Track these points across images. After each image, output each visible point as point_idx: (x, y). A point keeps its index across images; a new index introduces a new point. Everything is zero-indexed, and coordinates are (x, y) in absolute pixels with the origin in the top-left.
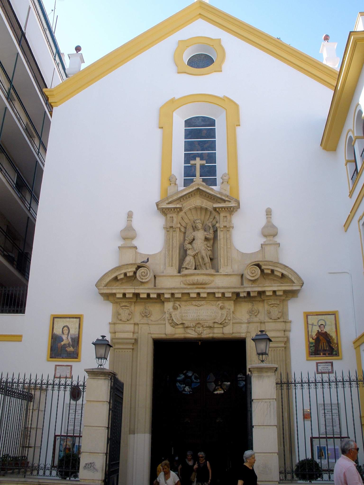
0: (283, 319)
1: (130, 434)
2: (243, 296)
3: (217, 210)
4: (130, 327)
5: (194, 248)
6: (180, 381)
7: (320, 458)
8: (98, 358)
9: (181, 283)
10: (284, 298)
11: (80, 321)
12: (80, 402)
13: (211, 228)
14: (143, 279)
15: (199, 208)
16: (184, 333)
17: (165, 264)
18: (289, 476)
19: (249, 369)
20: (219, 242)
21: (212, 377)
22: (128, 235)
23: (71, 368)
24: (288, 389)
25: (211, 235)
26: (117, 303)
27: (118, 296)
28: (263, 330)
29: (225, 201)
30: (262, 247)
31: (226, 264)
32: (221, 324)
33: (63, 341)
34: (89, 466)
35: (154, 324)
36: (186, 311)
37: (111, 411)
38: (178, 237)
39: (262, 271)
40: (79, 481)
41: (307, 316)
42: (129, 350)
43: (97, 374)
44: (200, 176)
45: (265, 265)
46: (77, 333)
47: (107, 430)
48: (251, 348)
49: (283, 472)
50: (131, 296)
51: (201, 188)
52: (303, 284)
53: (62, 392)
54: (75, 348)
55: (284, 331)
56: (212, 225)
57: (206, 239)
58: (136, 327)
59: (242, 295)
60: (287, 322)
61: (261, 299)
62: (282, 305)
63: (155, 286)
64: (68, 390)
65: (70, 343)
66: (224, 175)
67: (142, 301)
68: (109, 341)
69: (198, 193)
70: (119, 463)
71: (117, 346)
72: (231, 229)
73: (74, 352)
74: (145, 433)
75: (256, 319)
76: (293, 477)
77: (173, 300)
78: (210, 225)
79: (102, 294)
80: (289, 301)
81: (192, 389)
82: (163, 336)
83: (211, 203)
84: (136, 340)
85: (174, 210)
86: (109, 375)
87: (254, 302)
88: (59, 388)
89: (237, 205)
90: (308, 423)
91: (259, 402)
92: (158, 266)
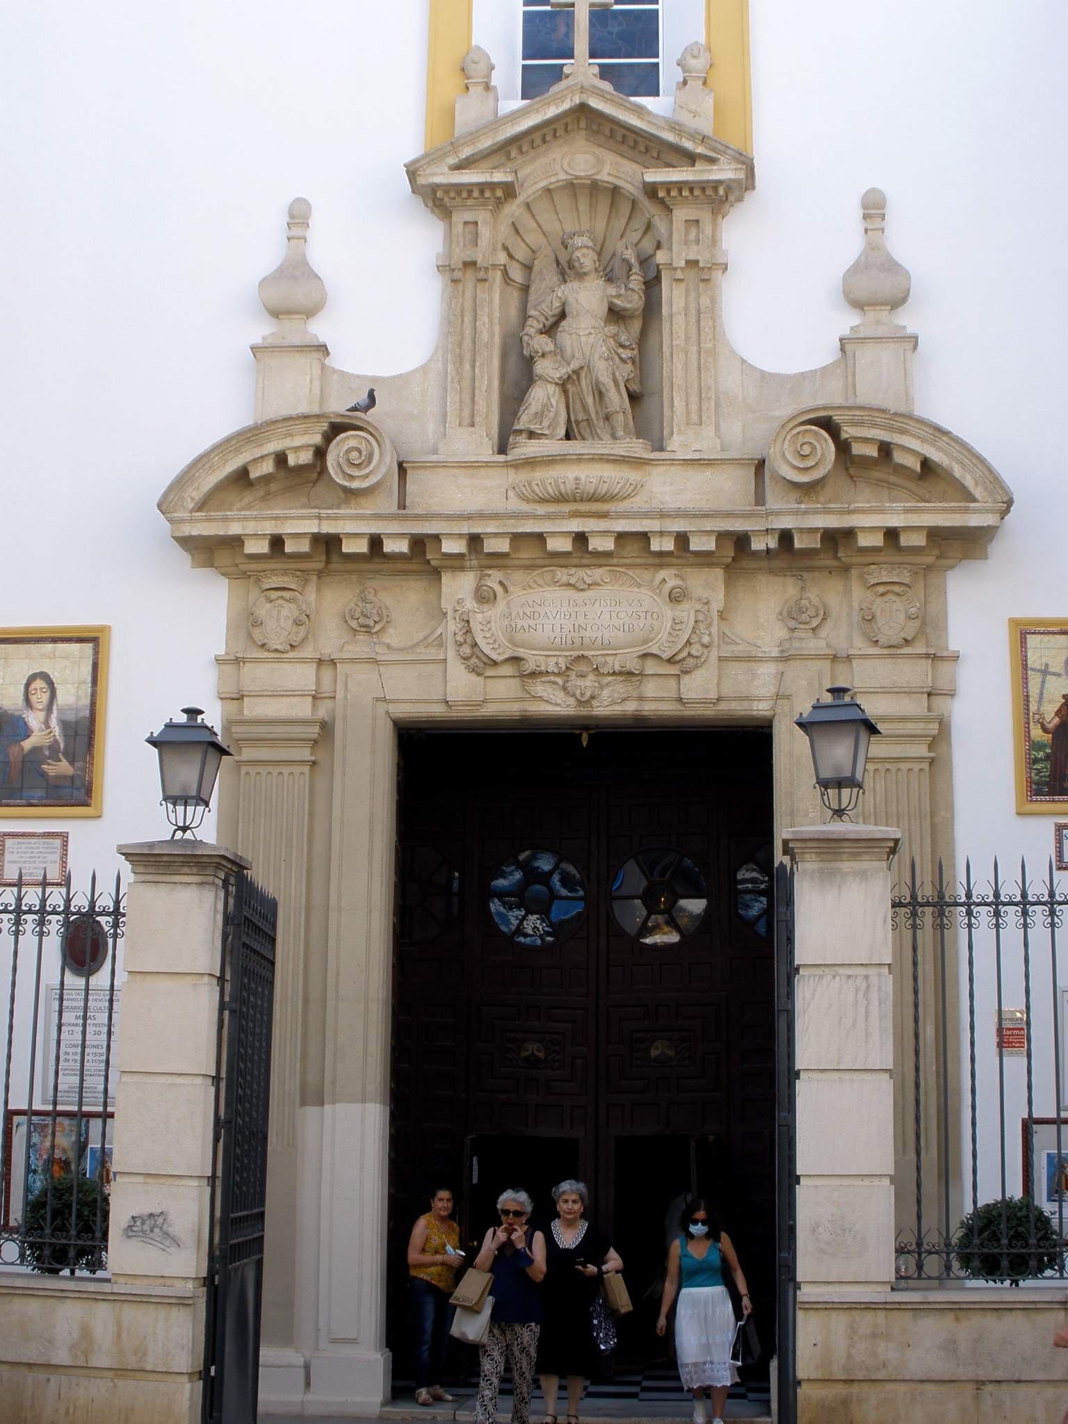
0: (925, 643)
1: (304, 1103)
2: (762, 547)
3: (661, 194)
4: (302, 676)
5: (562, 352)
6: (501, 895)
7: (1056, 1197)
8: (173, 799)
9: (511, 494)
10: (929, 560)
11: (96, 652)
12: (101, 979)
13: (636, 269)
14: (352, 477)
15: (582, 185)
16: (522, 700)
17: (444, 416)
18: (933, 1264)
19: (786, 842)
20: (666, 326)
21: (632, 877)
22: (292, 298)
23: (65, 845)
24: (940, 927)
25: (636, 297)
26: (245, 575)
27: (251, 547)
28: (844, 685)
29: (691, 158)
30: (843, 350)
31: (694, 417)
32: (670, 661)
33: (28, 736)
34: (146, 1227)
35: (395, 662)
36: (528, 610)
37: (226, 1013)
38: (496, 305)
39: (843, 447)
40: (108, 1281)
41: (1023, 635)
42: (297, 770)
43: (168, 864)
44: (592, 56)
45: (854, 424)
46: (86, 701)
47: (212, 1090)
48: (792, 758)
49: (913, 1253)
50: (304, 547)
51: (595, 103)
52: (1010, 503)
53: (29, 941)
54: (78, 764)
55: (929, 695)
56: (638, 256)
57: (615, 314)
58: (327, 673)
59: (757, 545)
60: (942, 658)
61: (834, 563)
62: (921, 585)
63: (402, 505)
64: (53, 933)
65: (56, 741)
66: (692, 51)
67: (349, 566)
68: (218, 730)
69: (583, 125)
70: (262, 1214)
71: (248, 753)
72: (717, 274)
73: (72, 777)
74: (364, 1101)
75: (814, 645)
76: (948, 1268)
77: (475, 563)
78: (630, 255)
79: (186, 542)
80: (950, 574)
81: (550, 926)
82: (437, 711)
83: (635, 166)
84: (326, 727)
85: (482, 192)
86: (218, 866)
87: (805, 575)
88: (17, 923)
89: (741, 175)
90: (1015, 1063)
91: (821, 977)
92: (415, 422)
